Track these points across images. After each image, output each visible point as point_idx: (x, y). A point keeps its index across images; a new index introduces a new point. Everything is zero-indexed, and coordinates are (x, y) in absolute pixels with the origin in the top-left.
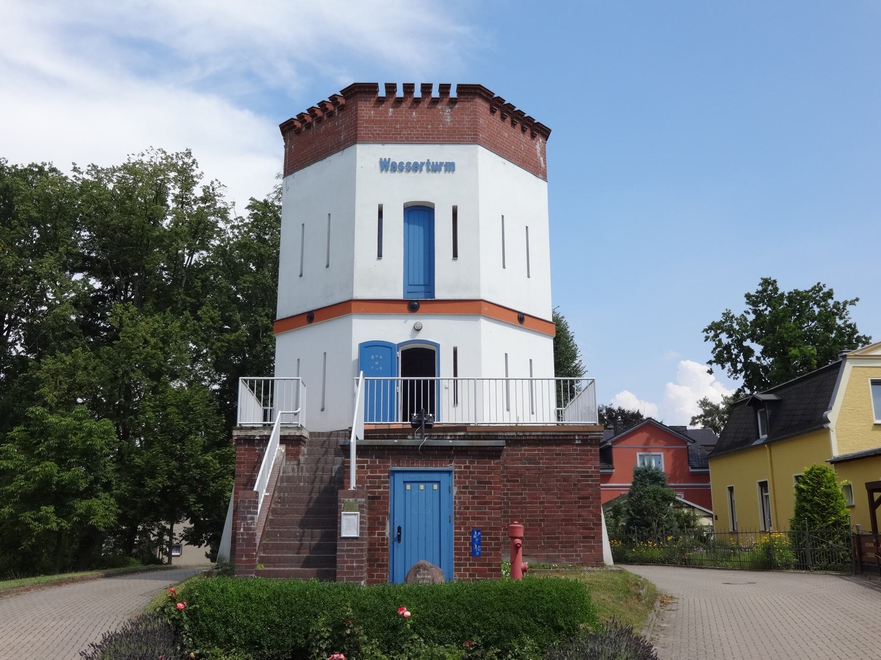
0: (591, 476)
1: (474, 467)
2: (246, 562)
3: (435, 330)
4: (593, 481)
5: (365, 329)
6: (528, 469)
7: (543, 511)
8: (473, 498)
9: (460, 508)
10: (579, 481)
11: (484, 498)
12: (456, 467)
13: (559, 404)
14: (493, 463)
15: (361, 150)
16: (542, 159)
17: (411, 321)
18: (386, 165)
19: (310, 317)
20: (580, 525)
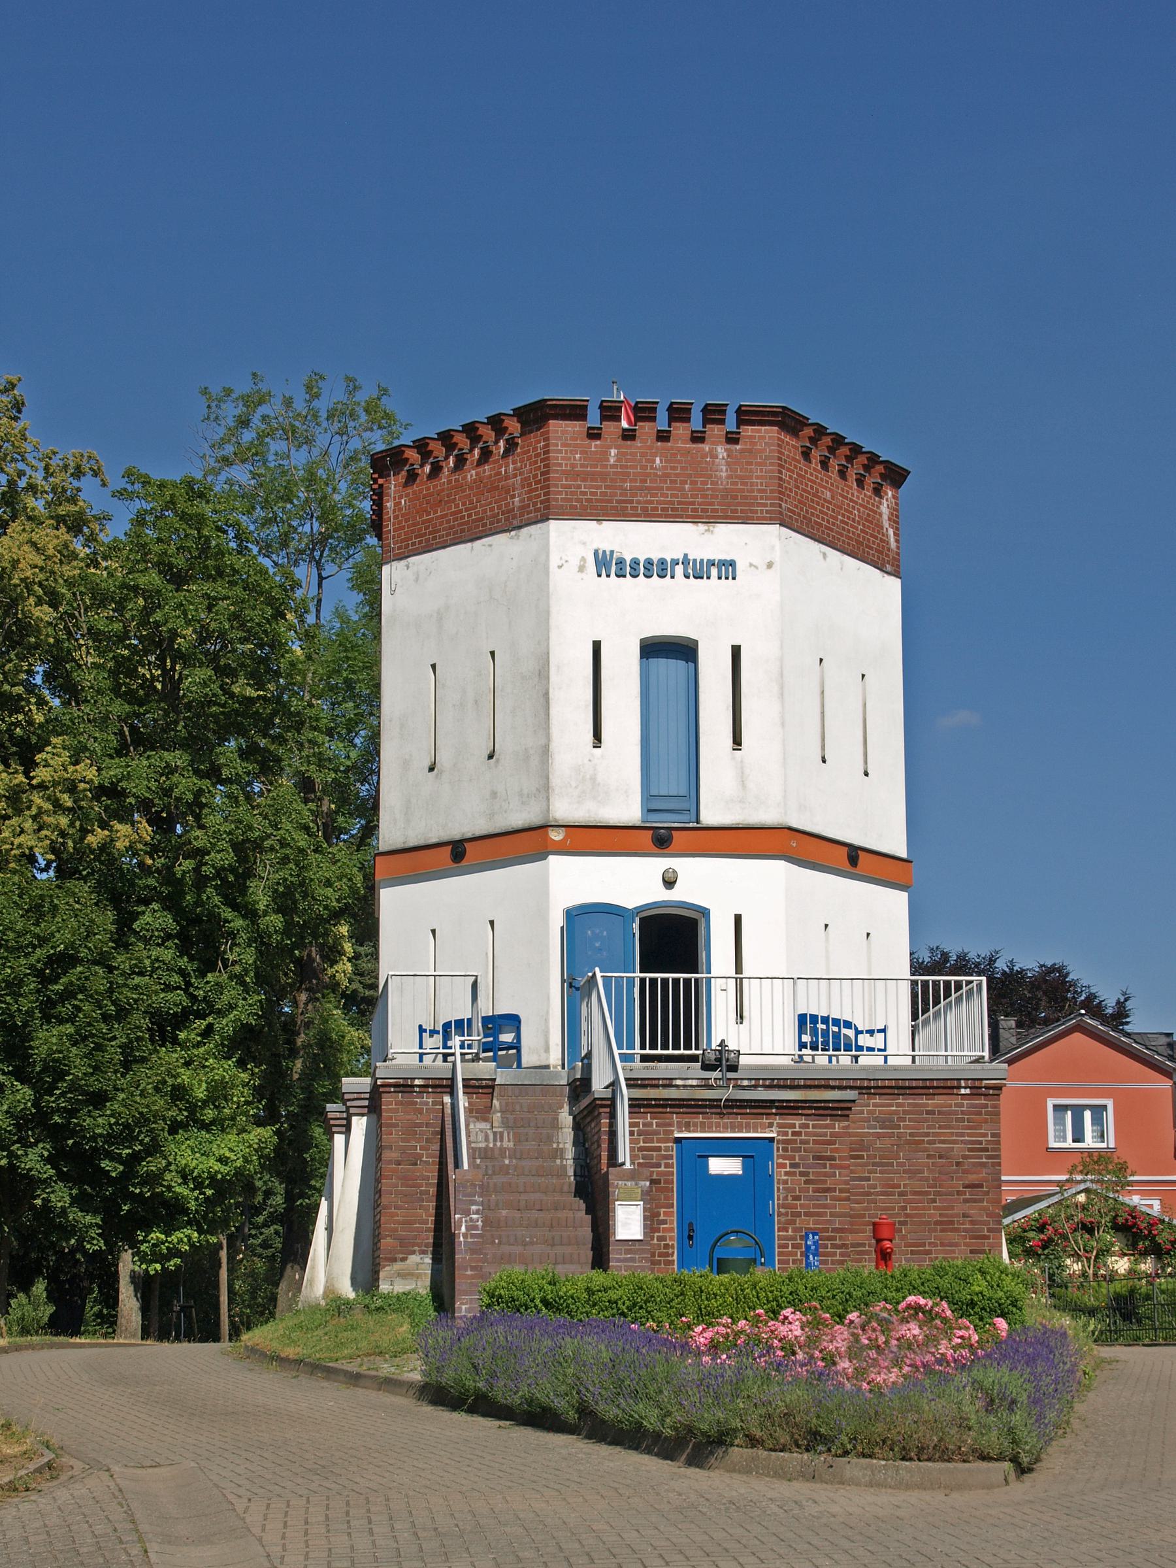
0: (987, 1150)
1: (807, 1134)
2: (472, 1277)
3: (703, 882)
4: (988, 1157)
5: (578, 880)
6: (878, 1136)
7: (905, 1208)
8: (806, 1182)
9: (786, 1198)
10: (965, 1157)
11: (825, 1182)
12: (779, 1133)
13: (915, 1017)
14: (838, 1126)
15: (557, 530)
16: (891, 532)
17: (657, 865)
18: (605, 563)
19: (459, 854)
20: (966, 1230)
